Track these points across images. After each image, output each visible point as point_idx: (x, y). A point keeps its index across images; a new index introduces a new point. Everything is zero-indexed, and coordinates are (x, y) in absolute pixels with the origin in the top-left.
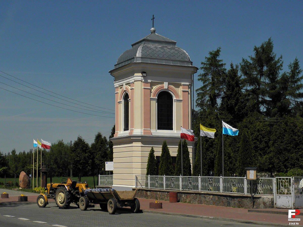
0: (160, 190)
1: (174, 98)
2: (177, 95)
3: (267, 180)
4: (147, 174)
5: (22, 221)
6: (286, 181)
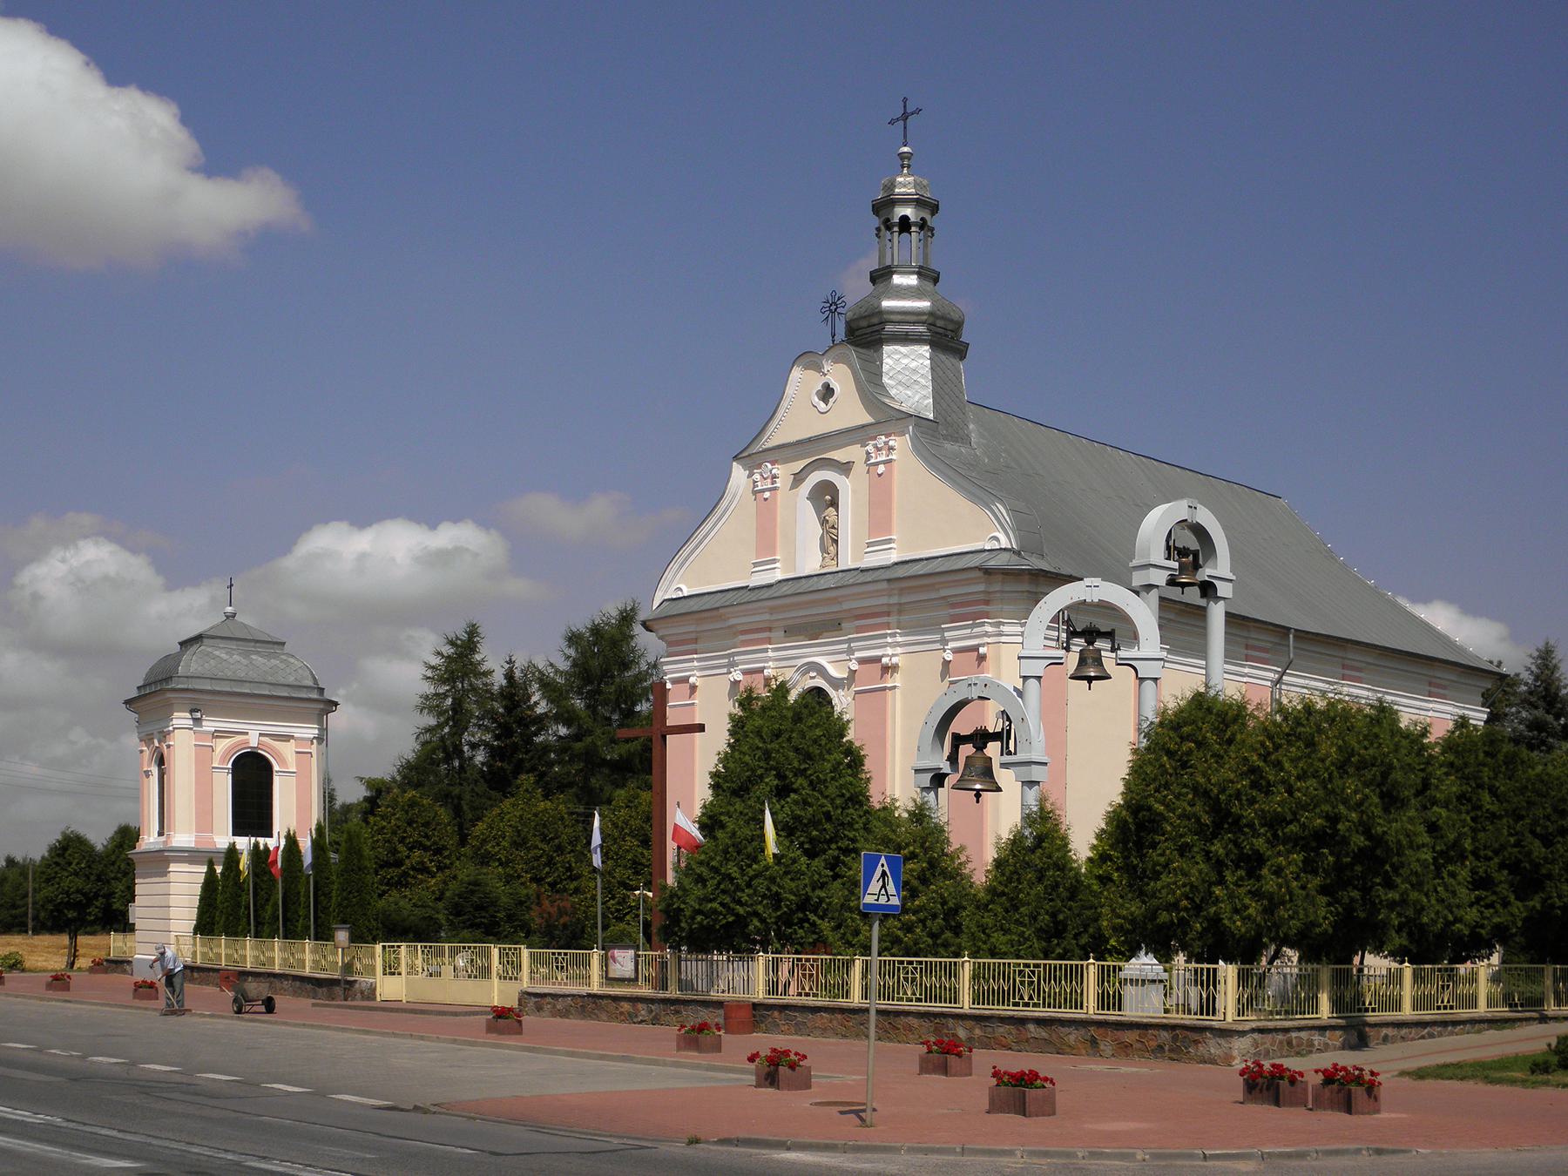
1: (276, 767)
2: (282, 762)
4: (195, 933)
5: (155, 1071)
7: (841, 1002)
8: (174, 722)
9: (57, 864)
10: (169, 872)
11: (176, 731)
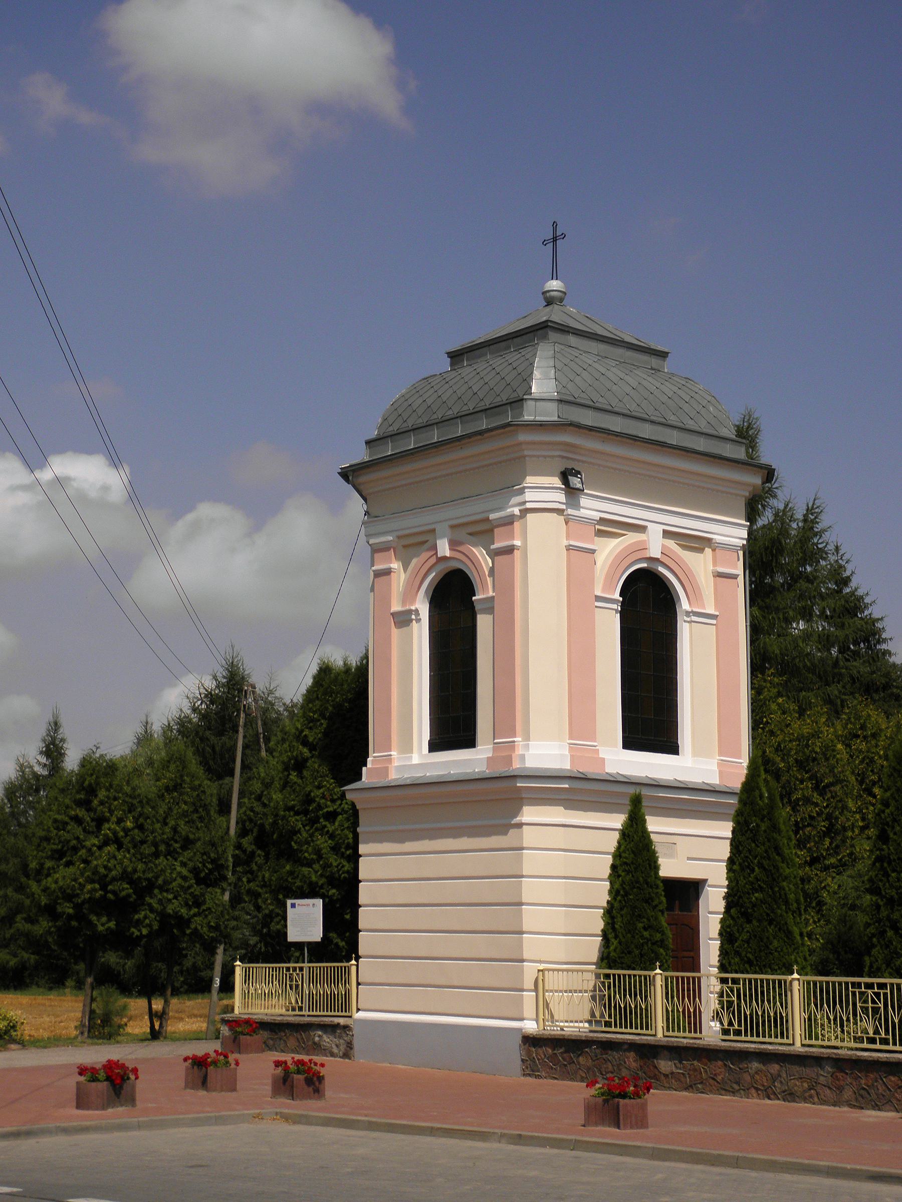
0: (309, 1019)
1: (685, 604)
3: (768, 984)
6: (877, 995)
7: (773, 1044)
8: (529, 495)
9: (78, 820)
10: (520, 825)
11: (530, 516)
